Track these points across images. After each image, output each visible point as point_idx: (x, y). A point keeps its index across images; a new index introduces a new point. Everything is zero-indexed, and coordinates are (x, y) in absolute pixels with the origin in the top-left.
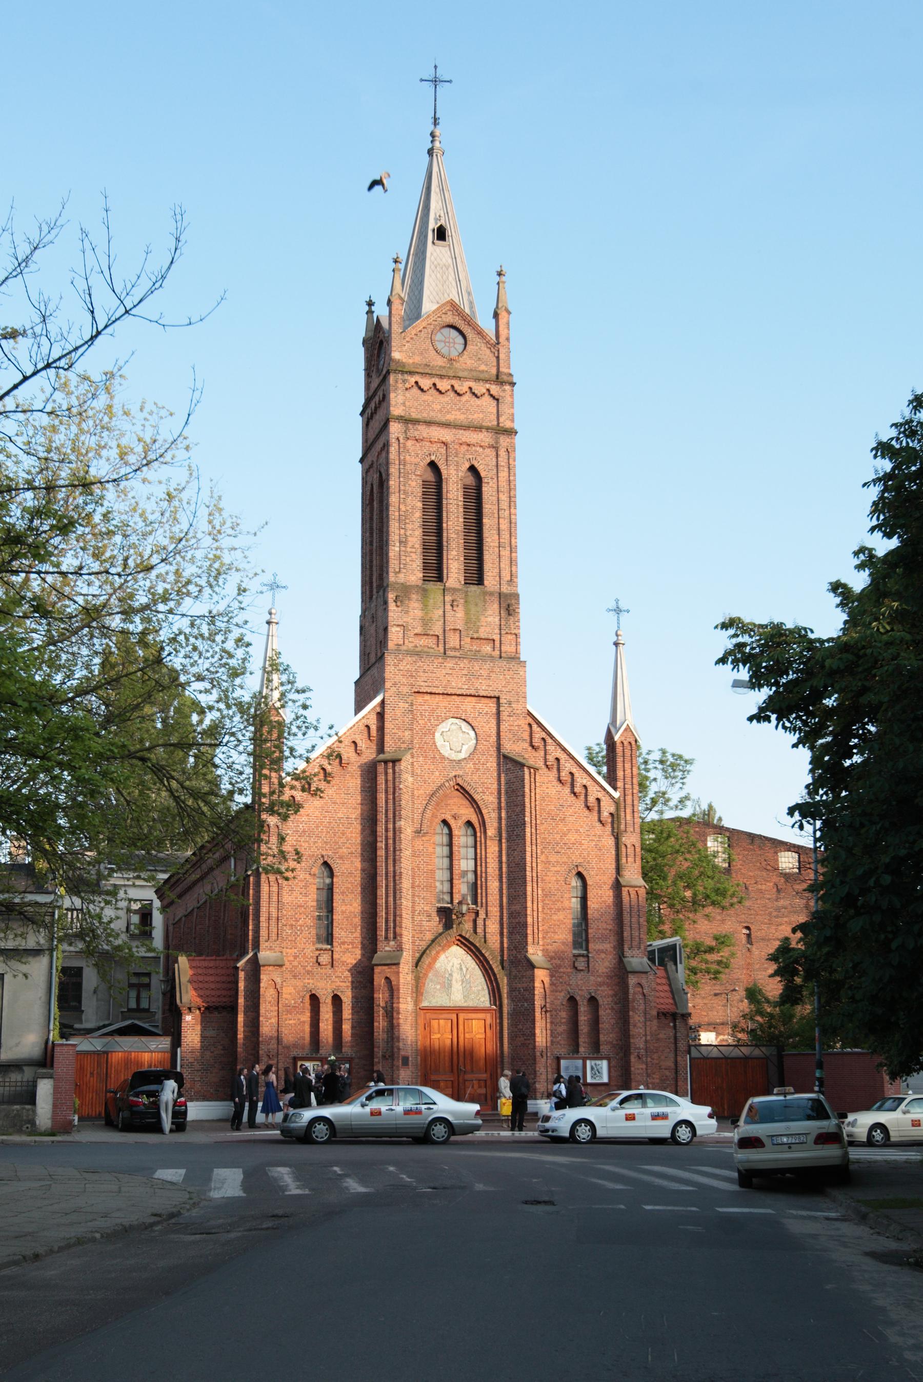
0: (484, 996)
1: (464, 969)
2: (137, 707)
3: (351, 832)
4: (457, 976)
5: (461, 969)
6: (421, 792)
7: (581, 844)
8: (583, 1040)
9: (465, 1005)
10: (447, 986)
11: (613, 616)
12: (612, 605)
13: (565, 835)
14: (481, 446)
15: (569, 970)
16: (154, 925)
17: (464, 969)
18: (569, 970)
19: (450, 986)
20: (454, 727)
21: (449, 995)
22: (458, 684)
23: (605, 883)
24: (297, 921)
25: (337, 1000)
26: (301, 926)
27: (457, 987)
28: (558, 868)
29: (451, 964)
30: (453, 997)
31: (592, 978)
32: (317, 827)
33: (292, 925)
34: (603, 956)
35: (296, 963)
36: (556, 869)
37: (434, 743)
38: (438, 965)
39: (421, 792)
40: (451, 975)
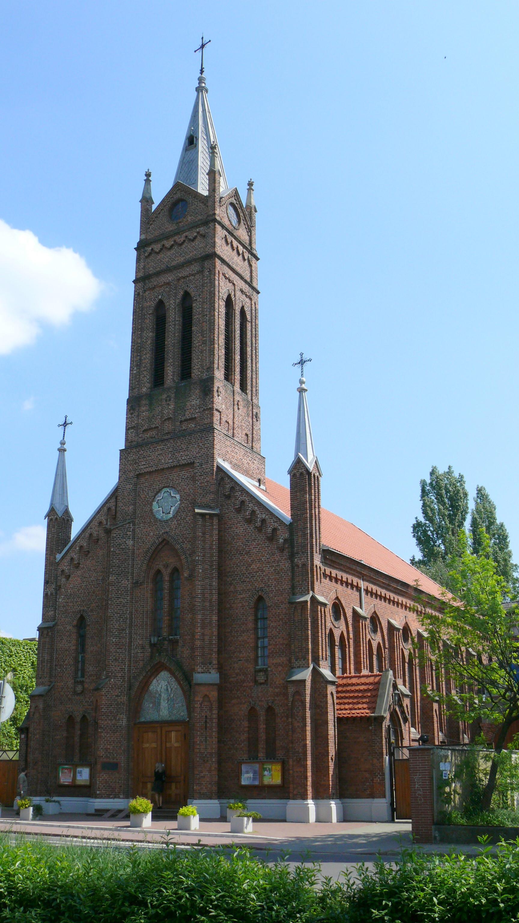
0: (183, 711)
1: (169, 690)
2: (136, 485)
3: (99, 591)
4: (164, 696)
5: (167, 689)
6: (141, 551)
7: (263, 571)
8: (262, 746)
9: (170, 719)
10: (157, 705)
11: (298, 368)
12: (305, 357)
13: (250, 565)
14: (192, 275)
15: (251, 684)
16: (412, 583)
17: (169, 690)
18: (251, 684)
19: (159, 704)
20: (166, 494)
21: (158, 711)
22: (167, 461)
23: (282, 602)
24: (64, 661)
25: (364, 668)
26: (66, 665)
27: (164, 704)
28: (244, 596)
29: (160, 686)
30: (161, 713)
31: (270, 690)
32: (78, 590)
33: (61, 665)
34: (280, 668)
35: (62, 693)
36: (242, 596)
37: (151, 510)
38: (151, 688)
39: (141, 551)
40: (160, 695)
